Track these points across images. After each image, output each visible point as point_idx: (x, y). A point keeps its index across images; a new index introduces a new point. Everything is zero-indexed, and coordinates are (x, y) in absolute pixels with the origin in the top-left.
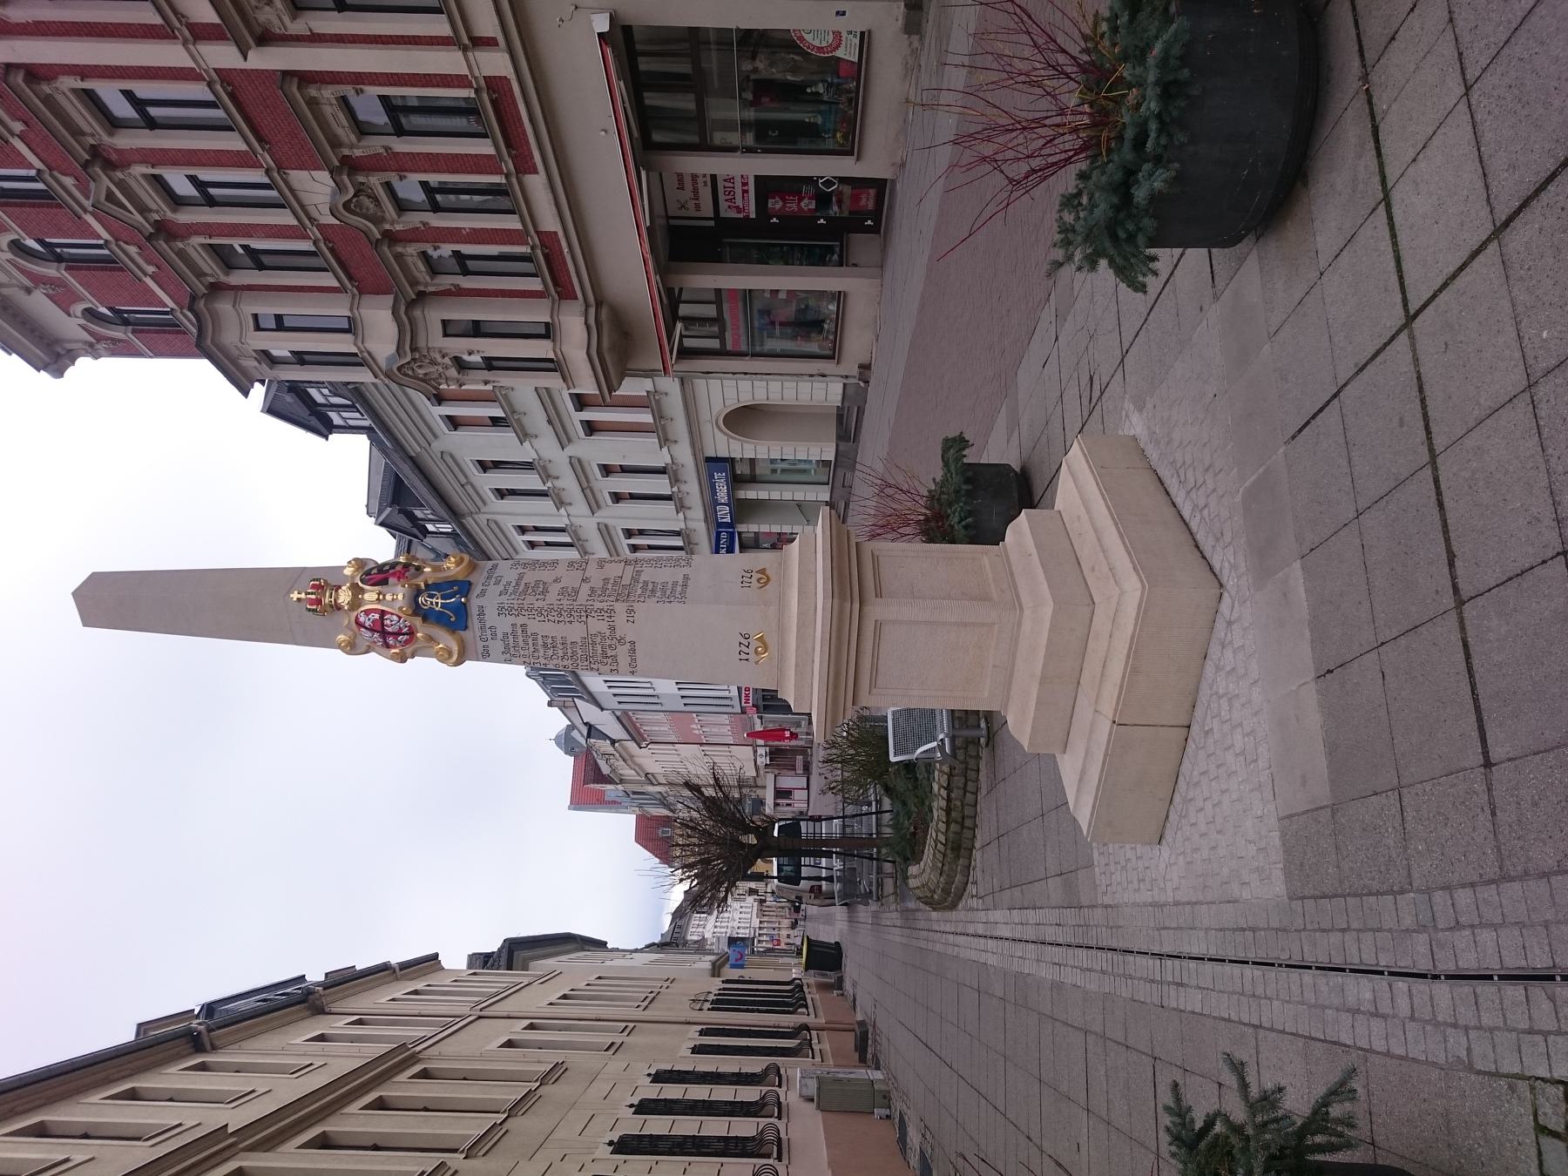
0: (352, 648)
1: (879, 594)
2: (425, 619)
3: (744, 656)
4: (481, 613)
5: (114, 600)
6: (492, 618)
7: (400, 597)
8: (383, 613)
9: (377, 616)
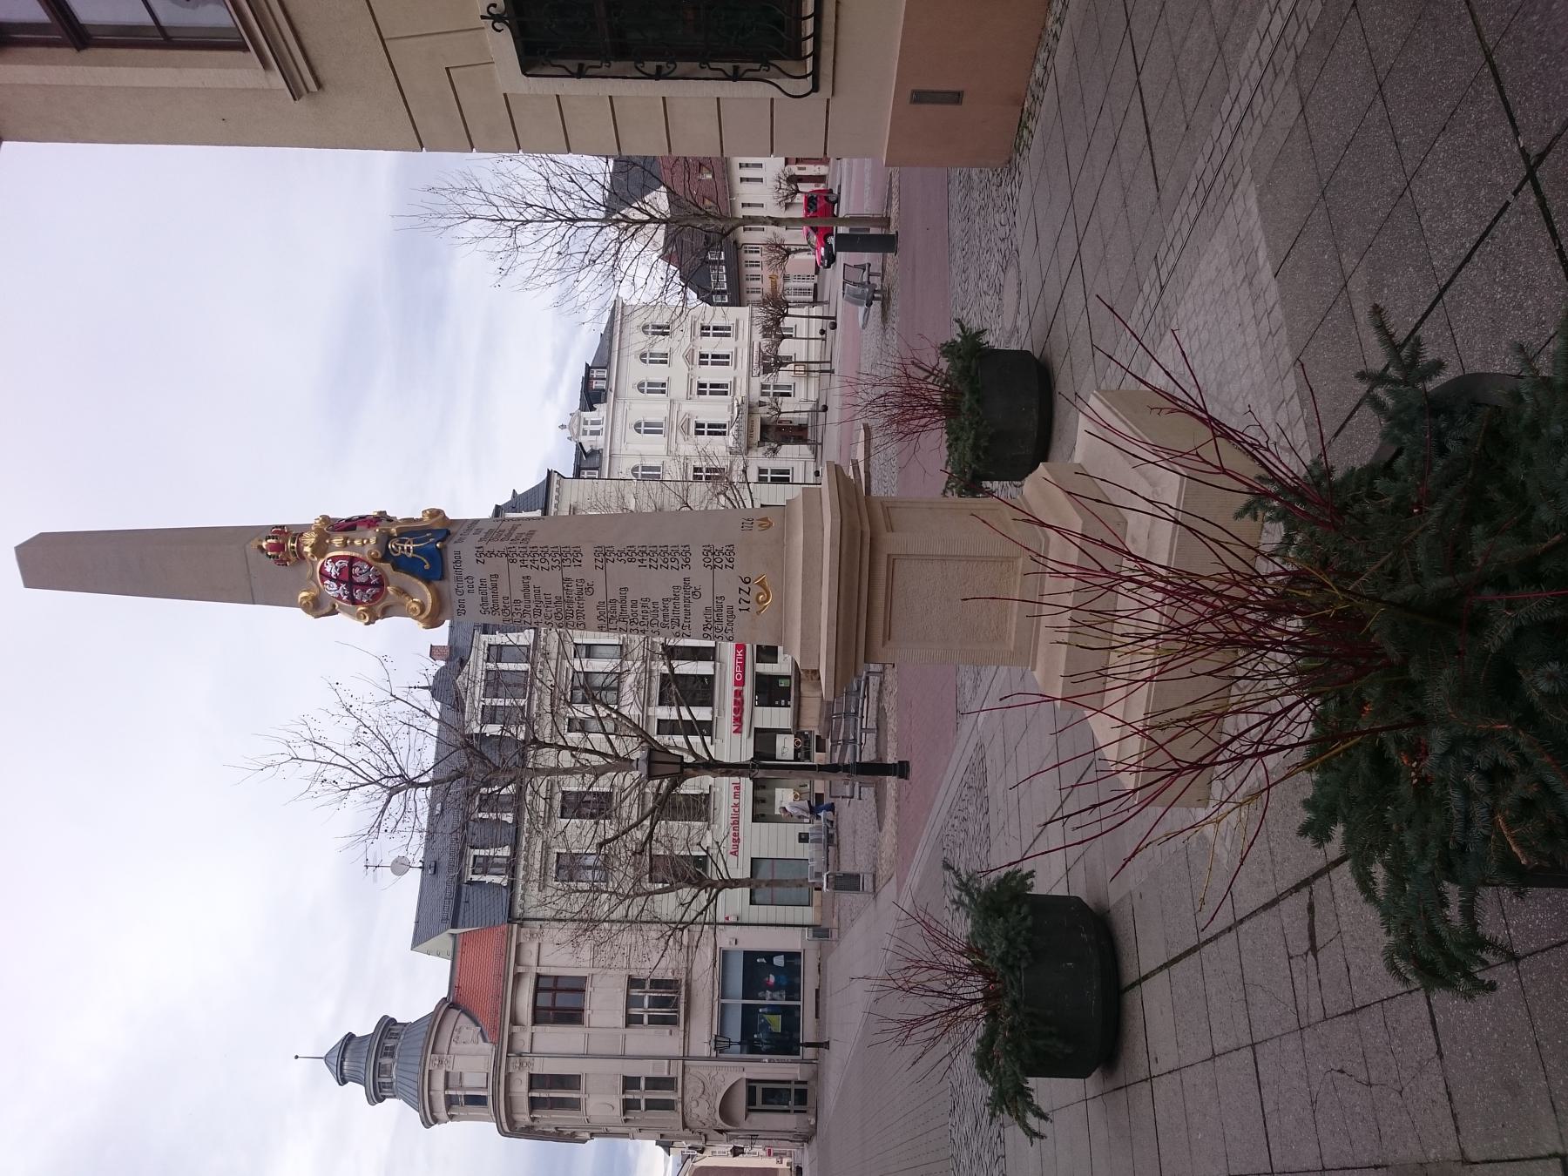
0: (317, 607)
1: (891, 528)
2: (396, 567)
3: (746, 606)
4: (458, 561)
5: (56, 561)
6: (470, 566)
7: (373, 541)
8: (352, 560)
9: (345, 563)
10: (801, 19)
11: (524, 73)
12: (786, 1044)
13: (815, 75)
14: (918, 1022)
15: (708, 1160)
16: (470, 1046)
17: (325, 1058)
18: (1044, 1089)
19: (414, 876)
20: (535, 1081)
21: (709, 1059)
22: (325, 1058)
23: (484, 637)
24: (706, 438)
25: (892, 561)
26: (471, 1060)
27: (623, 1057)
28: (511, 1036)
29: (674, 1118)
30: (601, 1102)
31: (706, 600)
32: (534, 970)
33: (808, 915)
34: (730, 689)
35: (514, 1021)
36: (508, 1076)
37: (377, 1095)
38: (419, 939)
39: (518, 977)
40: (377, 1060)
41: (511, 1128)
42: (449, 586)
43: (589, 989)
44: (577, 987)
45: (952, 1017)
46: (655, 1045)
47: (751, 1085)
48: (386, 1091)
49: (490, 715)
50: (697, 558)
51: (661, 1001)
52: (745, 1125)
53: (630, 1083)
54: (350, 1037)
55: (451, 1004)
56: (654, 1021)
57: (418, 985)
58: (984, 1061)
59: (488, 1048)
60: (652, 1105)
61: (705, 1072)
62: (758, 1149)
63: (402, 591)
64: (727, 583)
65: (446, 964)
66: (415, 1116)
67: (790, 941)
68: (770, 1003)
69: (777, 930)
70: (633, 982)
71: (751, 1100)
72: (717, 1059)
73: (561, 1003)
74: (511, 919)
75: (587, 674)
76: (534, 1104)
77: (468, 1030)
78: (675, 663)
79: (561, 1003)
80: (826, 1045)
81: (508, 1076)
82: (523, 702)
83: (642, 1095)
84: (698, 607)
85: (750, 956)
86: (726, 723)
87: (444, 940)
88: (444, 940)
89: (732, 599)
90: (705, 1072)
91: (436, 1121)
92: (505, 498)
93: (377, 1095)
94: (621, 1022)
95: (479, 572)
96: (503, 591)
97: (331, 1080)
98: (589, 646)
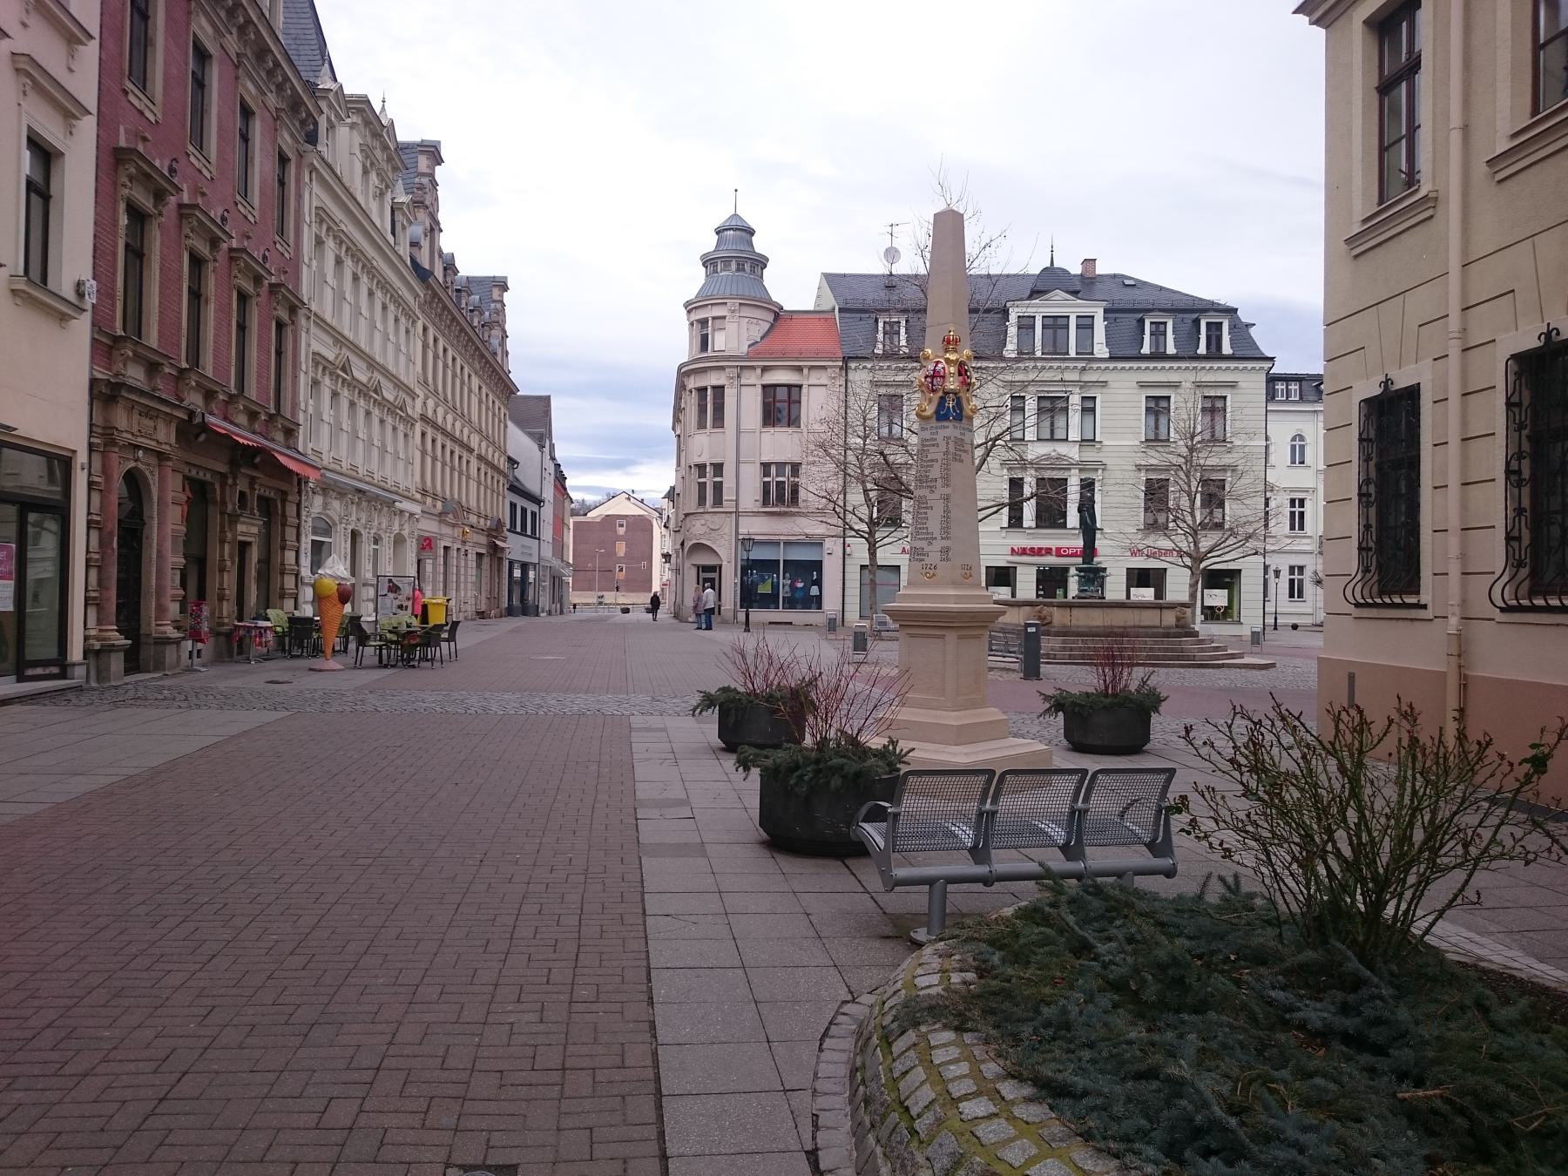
6: (943, 433)
10: (1400, 594)
11: (1513, 357)
12: (749, 598)
13: (1367, 605)
14: (744, 657)
15: (658, 531)
16: (745, 335)
17: (736, 215)
18: (713, 715)
19: (878, 267)
20: (719, 390)
21: (737, 533)
22: (736, 215)
23: (1101, 312)
24: (1287, 510)
25: (942, 637)
26: (731, 339)
27: (738, 462)
28: (753, 368)
29: (692, 506)
30: (704, 446)
31: (927, 549)
32: (805, 383)
33: (853, 615)
34: (1053, 543)
35: (765, 369)
36: (722, 368)
37: (709, 262)
38: (832, 280)
39: (799, 369)
40: (736, 257)
41: (684, 374)
42: (934, 423)
43: (790, 430)
44: (793, 421)
45: (746, 674)
46: (747, 488)
47: (716, 569)
48: (711, 268)
49: (1026, 325)
50: (946, 543)
51: (781, 493)
52: (687, 565)
53: (718, 468)
54: (751, 232)
55: (779, 315)
56: (766, 486)
57: (794, 285)
58: (725, 690)
59: (745, 349)
60: (702, 486)
61: (727, 530)
62: (668, 575)
63: (930, 401)
64: (934, 558)
65: (811, 308)
66: (692, 295)
67: (831, 603)
68: (780, 582)
69: (839, 589)
70: (796, 468)
71: (707, 569)
72: (737, 540)
73: (780, 408)
74: (846, 360)
75: (1067, 409)
76: (702, 391)
77: (757, 331)
78: (1033, 501)
79: (780, 408)
80: (747, 630)
81: (722, 368)
82: (1038, 354)
83: (709, 479)
84: (923, 544)
85: (818, 565)
86: (1020, 540)
87: (830, 302)
88: (830, 302)
89: (928, 561)
90: (727, 530)
91: (689, 312)
92: (1244, 317)
93: (709, 262)
94: (765, 459)
95: (940, 438)
96: (932, 449)
97: (718, 223)
98: (1093, 410)
